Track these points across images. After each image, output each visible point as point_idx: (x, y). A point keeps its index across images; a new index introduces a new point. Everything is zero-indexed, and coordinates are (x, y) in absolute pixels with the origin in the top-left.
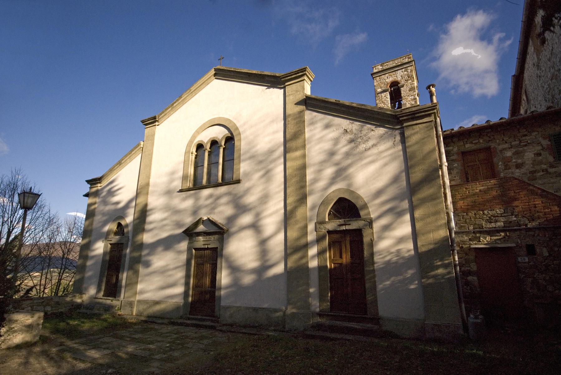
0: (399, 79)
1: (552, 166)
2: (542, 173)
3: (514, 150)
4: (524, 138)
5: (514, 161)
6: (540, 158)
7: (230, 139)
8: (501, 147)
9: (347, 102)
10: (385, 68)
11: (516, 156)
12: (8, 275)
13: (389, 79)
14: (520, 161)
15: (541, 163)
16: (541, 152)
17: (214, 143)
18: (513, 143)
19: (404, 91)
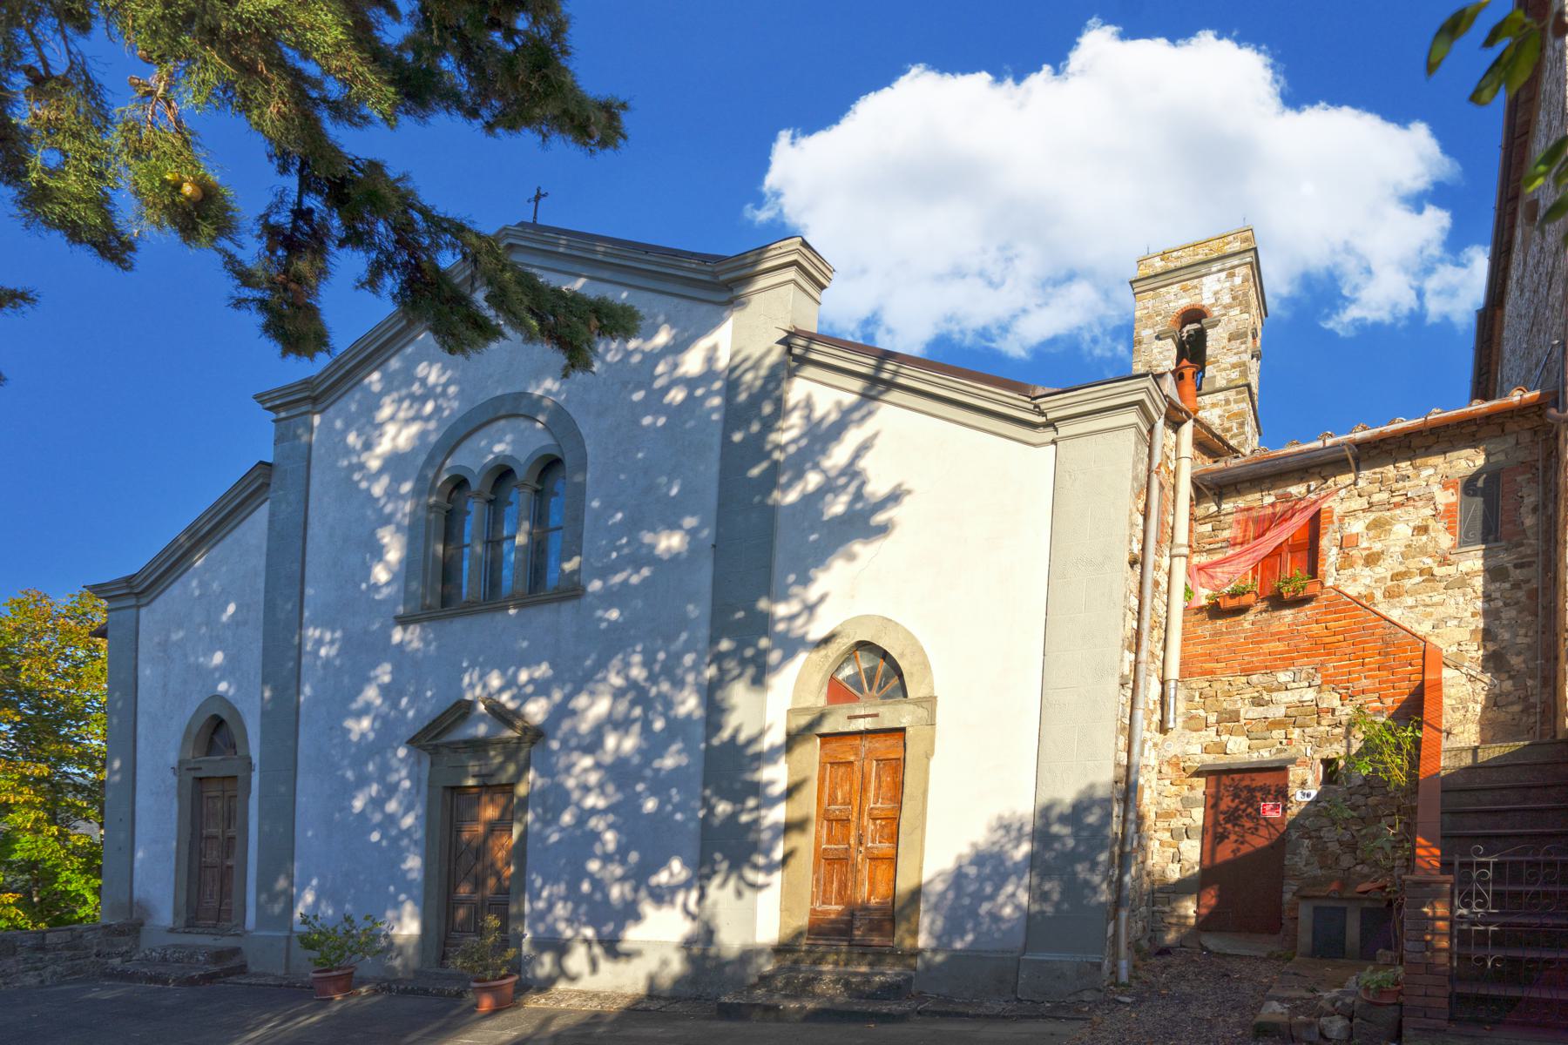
0: (1206, 300)
1: (1444, 561)
2: (1418, 579)
3: (1371, 516)
4: (1401, 484)
5: (1365, 545)
6: (1424, 538)
7: (550, 465)
8: (1339, 509)
9: (139, 756)
10: (1172, 266)
11: (1371, 534)
12: (670, 489)
13: (1177, 299)
14: (1377, 547)
15: (1423, 551)
16: (1431, 523)
17: (503, 474)
18: (1376, 498)
19: (1215, 340)
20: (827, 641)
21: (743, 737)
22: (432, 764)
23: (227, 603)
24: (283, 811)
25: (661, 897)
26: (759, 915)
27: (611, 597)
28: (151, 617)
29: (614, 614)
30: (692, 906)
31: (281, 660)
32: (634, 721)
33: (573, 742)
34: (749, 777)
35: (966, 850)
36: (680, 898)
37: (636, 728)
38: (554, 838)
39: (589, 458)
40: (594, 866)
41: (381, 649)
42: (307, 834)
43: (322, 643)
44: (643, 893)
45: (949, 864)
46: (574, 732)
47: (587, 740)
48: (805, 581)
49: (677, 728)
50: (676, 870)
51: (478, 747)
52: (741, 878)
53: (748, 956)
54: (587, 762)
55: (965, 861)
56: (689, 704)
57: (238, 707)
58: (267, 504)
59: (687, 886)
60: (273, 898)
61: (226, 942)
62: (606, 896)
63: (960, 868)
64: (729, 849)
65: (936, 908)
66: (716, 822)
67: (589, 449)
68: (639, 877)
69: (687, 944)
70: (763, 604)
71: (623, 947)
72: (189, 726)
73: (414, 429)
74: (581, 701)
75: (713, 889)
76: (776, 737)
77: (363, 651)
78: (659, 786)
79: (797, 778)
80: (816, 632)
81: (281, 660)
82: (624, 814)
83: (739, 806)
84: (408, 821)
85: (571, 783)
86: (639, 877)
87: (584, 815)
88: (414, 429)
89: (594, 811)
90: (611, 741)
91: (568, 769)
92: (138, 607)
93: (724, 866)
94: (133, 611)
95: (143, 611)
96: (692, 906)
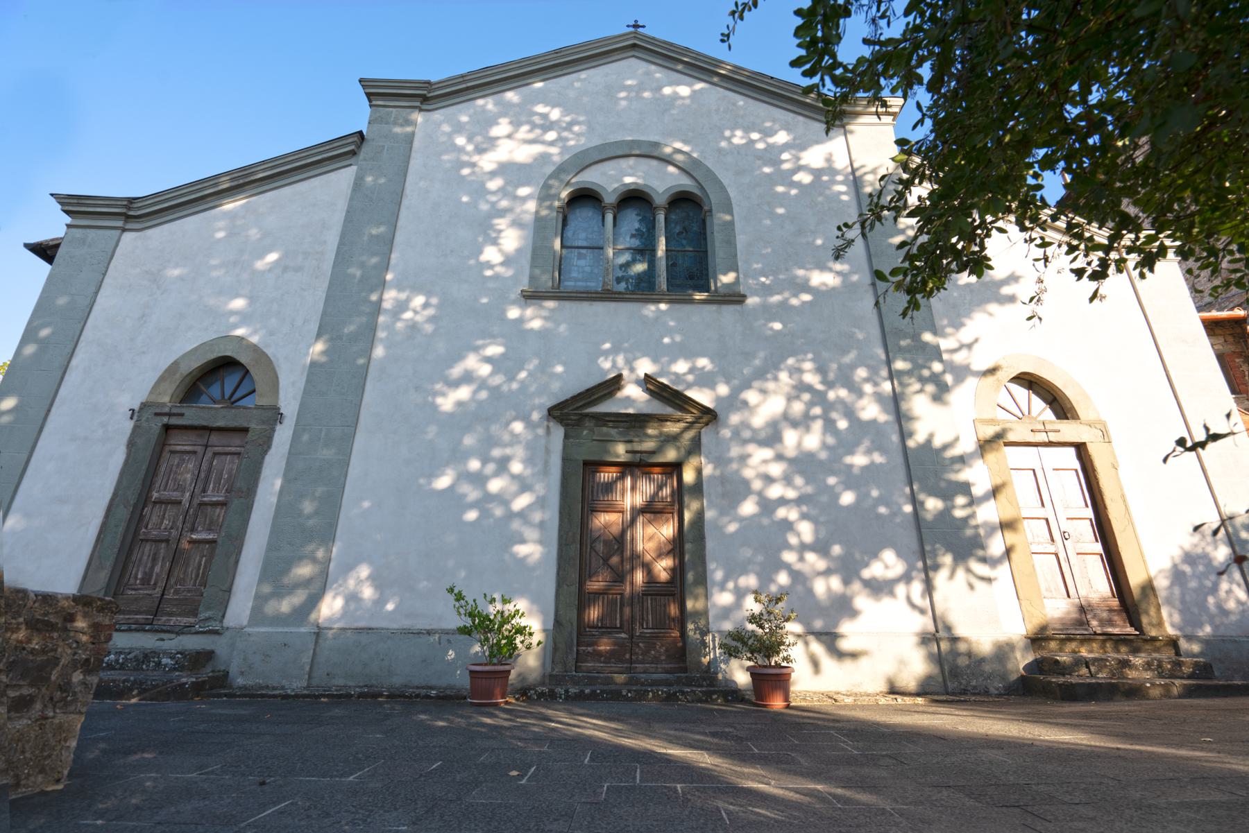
20: (992, 371)
21: (937, 443)
22: (566, 436)
23: (270, 251)
24: (323, 478)
25: (879, 588)
26: (994, 613)
27: (770, 312)
28: (133, 245)
29: (777, 326)
30: (918, 599)
31: (349, 311)
32: (815, 418)
33: (747, 434)
34: (953, 477)
35: (1177, 554)
36: (901, 589)
37: (818, 426)
38: (732, 528)
39: (733, 201)
40: (789, 557)
41: (488, 323)
42: (357, 506)
43: (408, 307)
44: (856, 586)
45: (1167, 565)
46: (745, 425)
47: (763, 435)
48: (958, 325)
49: (861, 428)
50: (888, 564)
51: (636, 423)
52: (969, 570)
53: (1003, 651)
54: (767, 453)
55: (1178, 560)
56: (870, 411)
57: (269, 352)
58: (354, 168)
59: (907, 578)
60: (281, 591)
61: (192, 643)
62: (810, 592)
63: (1175, 566)
64: (944, 541)
65: (1169, 601)
66: (929, 517)
67: (732, 195)
68: (849, 569)
69: (926, 639)
70: (928, 337)
71: (844, 645)
72: (176, 364)
73: (537, 149)
74: (751, 396)
75: (940, 578)
76: (967, 445)
77: (465, 321)
78: (852, 480)
79: (999, 481)
80: (979, 365)
81: (349, 311)
82: (816, 504)
83: (949, 503)
84: (521, 502)
85: (748, 473)
86: (849, 569)
87: (768, 506)
88: (537, 149)
89: (783, 501)
90: (791, 438)
91: (744, 458)
92: (124, 230)
93: (947, 559)
94: (118, 232)
95: (127, 237)
96: (918, 599)
